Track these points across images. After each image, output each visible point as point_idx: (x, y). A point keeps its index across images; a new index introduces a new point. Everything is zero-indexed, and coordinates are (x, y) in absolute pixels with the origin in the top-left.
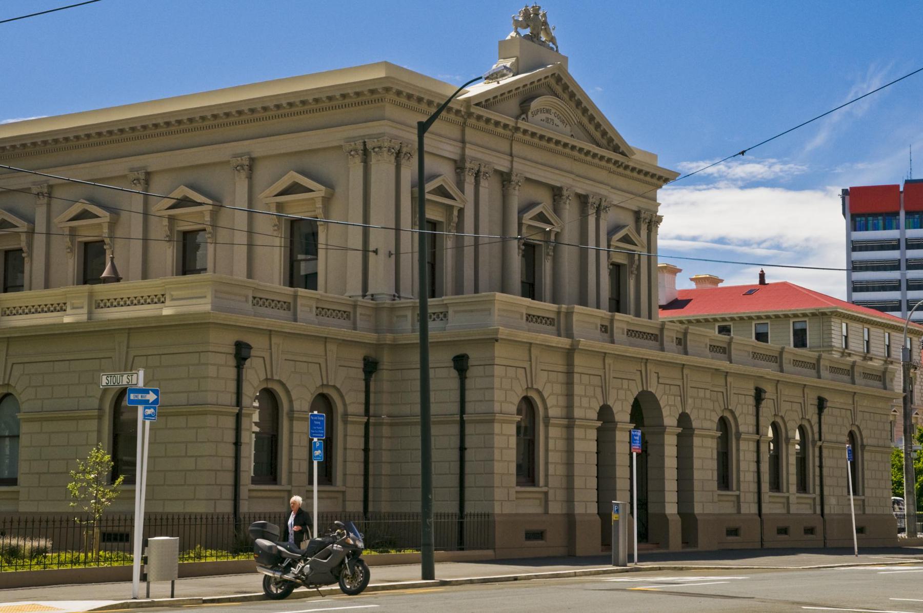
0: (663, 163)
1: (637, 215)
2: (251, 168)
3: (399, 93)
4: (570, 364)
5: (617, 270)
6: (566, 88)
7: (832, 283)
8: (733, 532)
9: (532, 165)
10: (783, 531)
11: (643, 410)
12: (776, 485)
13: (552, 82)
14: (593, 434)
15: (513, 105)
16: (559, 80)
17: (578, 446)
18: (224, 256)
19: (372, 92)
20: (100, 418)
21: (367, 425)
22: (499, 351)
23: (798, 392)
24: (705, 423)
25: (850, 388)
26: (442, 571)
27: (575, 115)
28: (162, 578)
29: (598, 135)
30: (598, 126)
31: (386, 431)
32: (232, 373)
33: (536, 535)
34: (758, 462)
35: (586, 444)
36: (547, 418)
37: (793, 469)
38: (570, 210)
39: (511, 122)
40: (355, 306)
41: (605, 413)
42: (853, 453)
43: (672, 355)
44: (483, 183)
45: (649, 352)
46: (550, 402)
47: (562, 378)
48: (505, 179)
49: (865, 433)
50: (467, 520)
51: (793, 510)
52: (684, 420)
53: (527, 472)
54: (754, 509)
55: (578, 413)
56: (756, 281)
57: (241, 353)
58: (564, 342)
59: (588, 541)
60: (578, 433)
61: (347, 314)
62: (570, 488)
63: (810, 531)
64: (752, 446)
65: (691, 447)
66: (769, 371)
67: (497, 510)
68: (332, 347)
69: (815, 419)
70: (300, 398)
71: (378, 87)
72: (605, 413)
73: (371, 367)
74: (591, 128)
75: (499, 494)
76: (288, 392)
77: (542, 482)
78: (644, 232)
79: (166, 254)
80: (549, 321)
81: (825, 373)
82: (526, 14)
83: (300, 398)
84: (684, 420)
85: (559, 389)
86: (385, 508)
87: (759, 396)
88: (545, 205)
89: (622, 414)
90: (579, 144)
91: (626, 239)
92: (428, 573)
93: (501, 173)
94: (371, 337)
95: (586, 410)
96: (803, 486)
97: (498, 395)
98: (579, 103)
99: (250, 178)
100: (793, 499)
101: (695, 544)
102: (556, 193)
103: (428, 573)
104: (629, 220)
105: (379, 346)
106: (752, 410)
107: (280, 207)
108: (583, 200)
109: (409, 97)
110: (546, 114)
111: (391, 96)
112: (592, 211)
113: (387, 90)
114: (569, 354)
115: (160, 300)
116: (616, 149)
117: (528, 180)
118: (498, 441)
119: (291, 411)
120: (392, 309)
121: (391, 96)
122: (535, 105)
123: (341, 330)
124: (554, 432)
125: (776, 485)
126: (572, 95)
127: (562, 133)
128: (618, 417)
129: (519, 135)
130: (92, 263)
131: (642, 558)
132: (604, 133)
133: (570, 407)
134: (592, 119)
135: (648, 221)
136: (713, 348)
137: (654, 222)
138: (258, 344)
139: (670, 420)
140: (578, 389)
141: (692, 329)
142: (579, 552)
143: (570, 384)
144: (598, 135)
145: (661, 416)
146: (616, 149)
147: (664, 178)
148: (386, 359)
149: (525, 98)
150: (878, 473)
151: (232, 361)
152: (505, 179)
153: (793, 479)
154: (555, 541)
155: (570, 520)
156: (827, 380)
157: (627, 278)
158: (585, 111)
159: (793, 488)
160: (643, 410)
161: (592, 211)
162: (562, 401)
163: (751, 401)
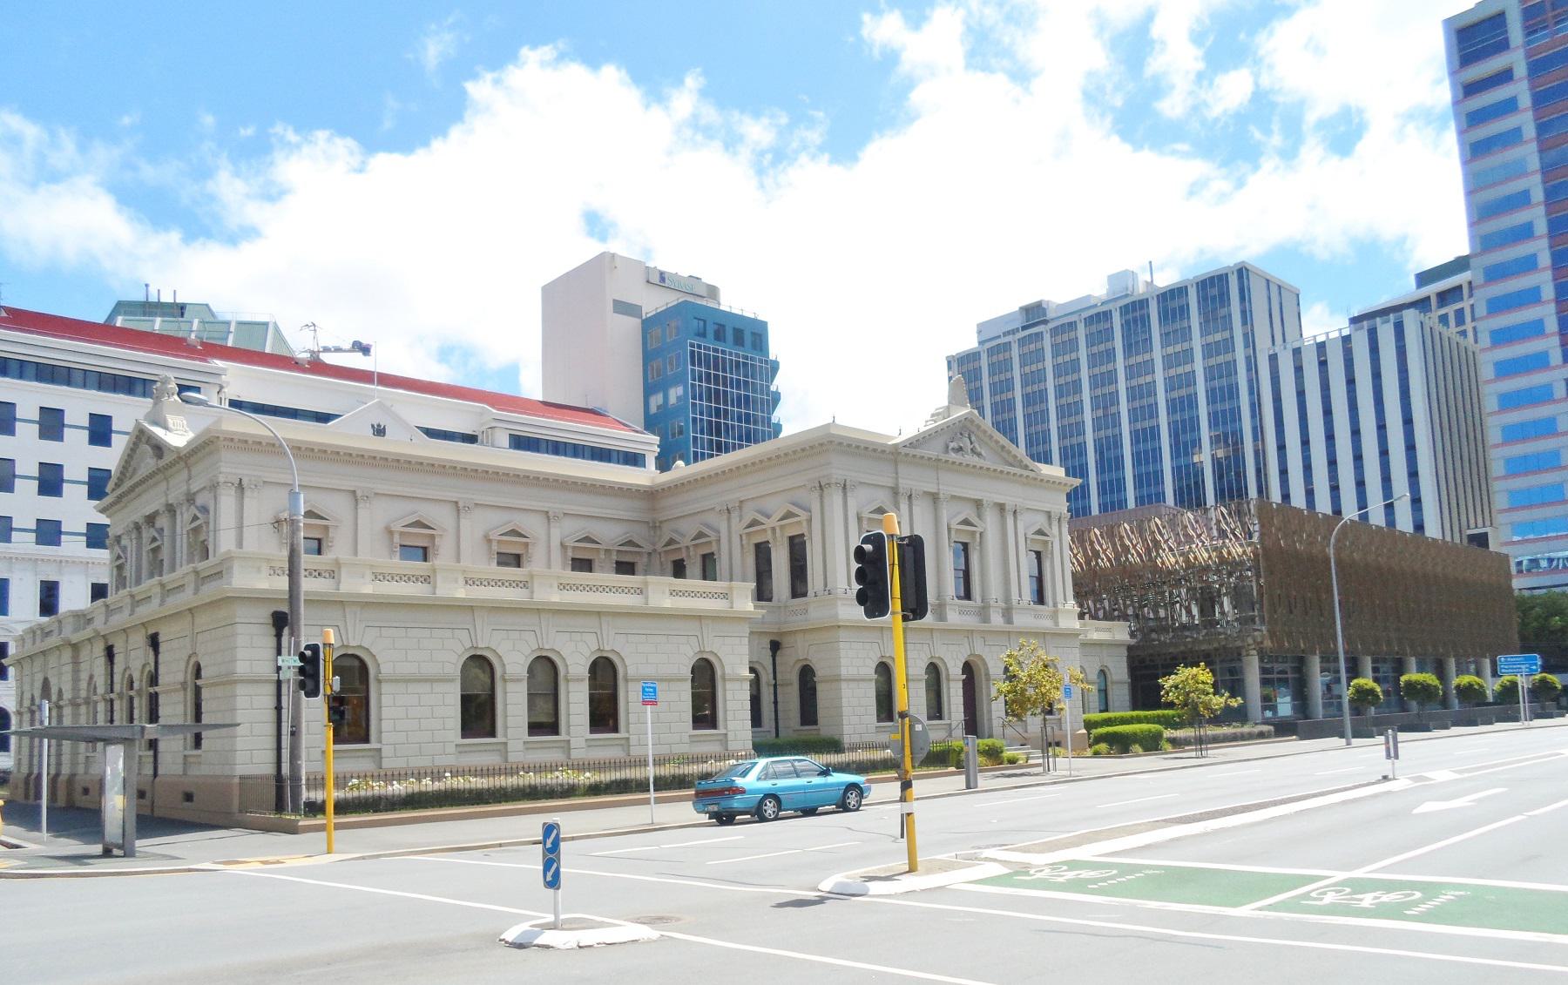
102: (978, 504)
108: (1001, 508)
117: (953, 497)
144: (1011, 460)
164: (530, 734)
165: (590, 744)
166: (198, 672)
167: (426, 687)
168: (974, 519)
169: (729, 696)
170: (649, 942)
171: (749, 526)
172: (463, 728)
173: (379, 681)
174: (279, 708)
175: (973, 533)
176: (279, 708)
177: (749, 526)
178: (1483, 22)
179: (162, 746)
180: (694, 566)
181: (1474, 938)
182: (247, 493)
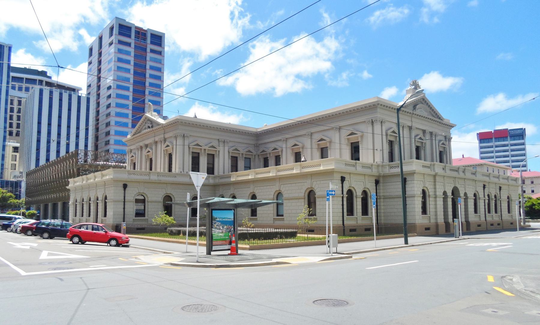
0: (452, 122)
1: (445, 137)
2: (311, 135)
3: (381, 105)
4: (435, 179)
5: (441, 153)
6: (426, 102)
7: (476, 155)
8: (479, 226)
9: (418, 124)
10: (492, 225)
11: (455, 192)
12: (489, 212)
13: (422, 100)
14: (442, 199)
15: (411, 107)
16: (424, 99)
17: (438, 203)
18: (333, 154)
19: (374, 105)
20: (304, 199)
21: (377, 199)
22: (416, 177)
23: (494, 185)
24: (471, 195)
25: (508, 183)
26: (410, 239)
27: (428, 109)
28: (333, 247)
29: (434, 115)
30: (435, 112)
31: (382, 200)
32: (341, 185)
33: (427, 229)
34: (485, 206)
35: (440, 202)
36: (429, 196)
37: (494, 207)
38: (428, 136)
39: (412, 112)
40: (372, 165)
41: (445, 193)
42: (509, 202)
43: (462, 175)
44: (405, 129)
45: (455, 174)
46: (430, 190)
47: (433, 183)
48: (410, 128)
49: (512, 196)
50: (439, 228)
51: (494, 218)
52: (465, 194)
53: (424, 211)
54: (484, 219)
55: (438, 193)
56: (462, 157)
57: (343, 179)
58: (433, 173)
59: (442, 229)
60: (438, 199)
61: (370, 167)
62: (436, 215)
63: (499, 224)
64: (483, 201)
65: (467, 202)
66: (486, 179)
67: (417, 222)
68: (366, 177)
69: (499, 193)
70: (358, 193)
71: (376, 104)
72: (445, 193)
73: (377, 182)
74: (433, 113)
75: (417, 217)
76: (355, 190)
77: (428, 213)
78: (447, 142)
79: (317, 154)
80: (429, 167)
81: (501, 180)
82: (413, 82)
83: (358, 193)
84: (465, 194)
85: (432, 187)
86: (383, 222)
87: (484, 187)
88: (421, 135)
89: (449, 193)
90: (428, 117)
91: (443, 144)
92: (406, 242)
93: (409, 127)
94: (377, 174)
95: (440, 193)
96: (496, 212)
97: (416, 189)
98: (429, 106)
99: (311, 138)
100: (494, 216)
101: (470, 230)
102: (424, 132)
103: (406, 242)
104: (443, 139)
105: (379, 176)
106: (483, 191)
107: (318, 145)
108: (431, 133)
109: (384, 106)
110: (421, 110)
111: (379, 106)
112: (434, 136)
113: (378, 104)
114: (435, 176)
115: (293, 169)
116: (440, 118)
117: (417, 128)
118: (416, 202)
119: (356, 195)
120: (382, 166)
121: (379, 106)
122: (418, 107)
123: (368, 171)
124: (431, 199)
125: (489, 212)
126: (427, 104)
127: (425, 114)
128: (448, 194)
129: (414, 115)
130: (298, 158)
131: (463, 234)
132: (436, 114)
133: (435, 192)
134: (433, 110)
135: (448, 139)
136: (472, 174)
137: (450, 139)
138: (347, 177)
139: (462, 195)
140: (437, 187)
141: (467, 168)
142: (440, 233)
143: (435, 185)
144: (434, 115)
145: (459, 194)
146: (440, 118)
147: (452, 126)
148: (381, 180)
149: (415, 105)
150: (515, 208)
151: (340, 182)
152: (410, 128)
153: (494, 210)
154: (433, 230)
155: (437, 225)
156: (502, 181)
157: (443, 155)
158: (431, 108)
159: (494, 212)
160: (455, 192)
161: (434, 136)
162: (433, 190)
163: (482, 188)
164: (135, 217)
165: (363, 219)
166: (106, 198)
167: (297, 201)
168: (423, 138)
169: (149, 207)
170: (509, 296)
171: (273, 150)
172: (362, 213)
173: (304, 199)
174: (343, 205)
175: (422, 143)
176: (343, 205)
177: (273, 150)
178: (124, 26)
179: (122, 220)
180: (272, 161)
181: (3, 262)
182: (375, 124)
